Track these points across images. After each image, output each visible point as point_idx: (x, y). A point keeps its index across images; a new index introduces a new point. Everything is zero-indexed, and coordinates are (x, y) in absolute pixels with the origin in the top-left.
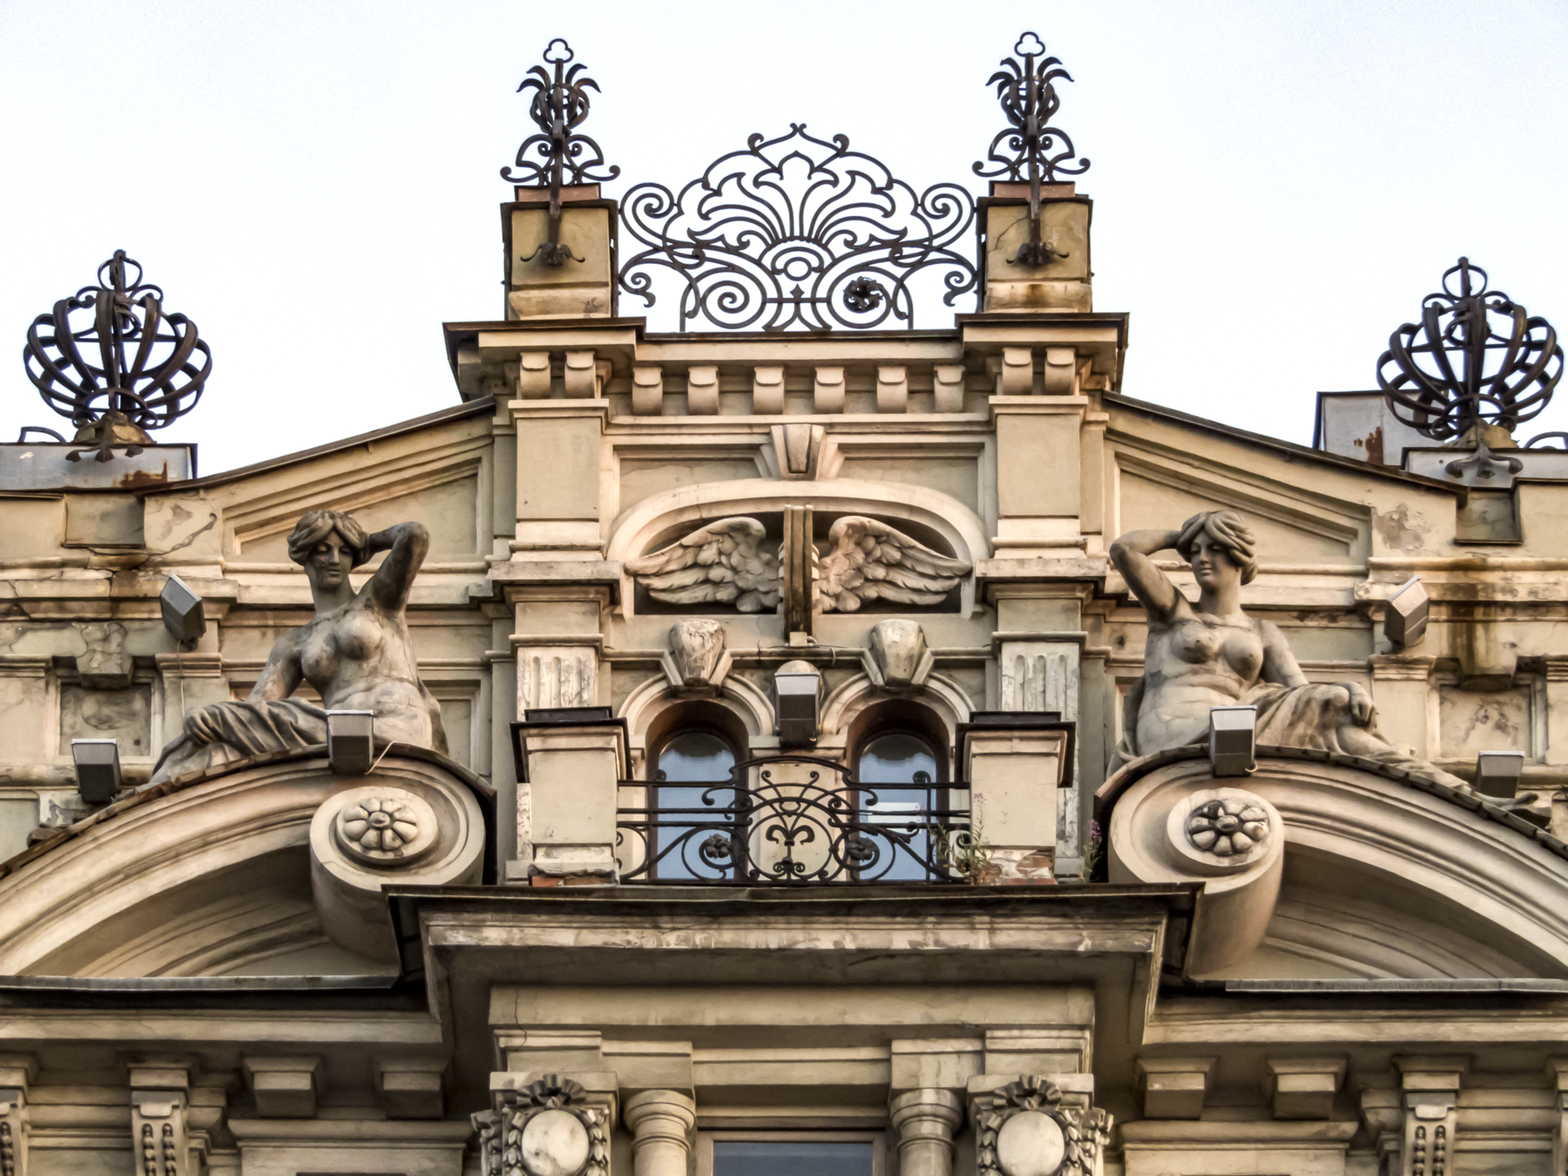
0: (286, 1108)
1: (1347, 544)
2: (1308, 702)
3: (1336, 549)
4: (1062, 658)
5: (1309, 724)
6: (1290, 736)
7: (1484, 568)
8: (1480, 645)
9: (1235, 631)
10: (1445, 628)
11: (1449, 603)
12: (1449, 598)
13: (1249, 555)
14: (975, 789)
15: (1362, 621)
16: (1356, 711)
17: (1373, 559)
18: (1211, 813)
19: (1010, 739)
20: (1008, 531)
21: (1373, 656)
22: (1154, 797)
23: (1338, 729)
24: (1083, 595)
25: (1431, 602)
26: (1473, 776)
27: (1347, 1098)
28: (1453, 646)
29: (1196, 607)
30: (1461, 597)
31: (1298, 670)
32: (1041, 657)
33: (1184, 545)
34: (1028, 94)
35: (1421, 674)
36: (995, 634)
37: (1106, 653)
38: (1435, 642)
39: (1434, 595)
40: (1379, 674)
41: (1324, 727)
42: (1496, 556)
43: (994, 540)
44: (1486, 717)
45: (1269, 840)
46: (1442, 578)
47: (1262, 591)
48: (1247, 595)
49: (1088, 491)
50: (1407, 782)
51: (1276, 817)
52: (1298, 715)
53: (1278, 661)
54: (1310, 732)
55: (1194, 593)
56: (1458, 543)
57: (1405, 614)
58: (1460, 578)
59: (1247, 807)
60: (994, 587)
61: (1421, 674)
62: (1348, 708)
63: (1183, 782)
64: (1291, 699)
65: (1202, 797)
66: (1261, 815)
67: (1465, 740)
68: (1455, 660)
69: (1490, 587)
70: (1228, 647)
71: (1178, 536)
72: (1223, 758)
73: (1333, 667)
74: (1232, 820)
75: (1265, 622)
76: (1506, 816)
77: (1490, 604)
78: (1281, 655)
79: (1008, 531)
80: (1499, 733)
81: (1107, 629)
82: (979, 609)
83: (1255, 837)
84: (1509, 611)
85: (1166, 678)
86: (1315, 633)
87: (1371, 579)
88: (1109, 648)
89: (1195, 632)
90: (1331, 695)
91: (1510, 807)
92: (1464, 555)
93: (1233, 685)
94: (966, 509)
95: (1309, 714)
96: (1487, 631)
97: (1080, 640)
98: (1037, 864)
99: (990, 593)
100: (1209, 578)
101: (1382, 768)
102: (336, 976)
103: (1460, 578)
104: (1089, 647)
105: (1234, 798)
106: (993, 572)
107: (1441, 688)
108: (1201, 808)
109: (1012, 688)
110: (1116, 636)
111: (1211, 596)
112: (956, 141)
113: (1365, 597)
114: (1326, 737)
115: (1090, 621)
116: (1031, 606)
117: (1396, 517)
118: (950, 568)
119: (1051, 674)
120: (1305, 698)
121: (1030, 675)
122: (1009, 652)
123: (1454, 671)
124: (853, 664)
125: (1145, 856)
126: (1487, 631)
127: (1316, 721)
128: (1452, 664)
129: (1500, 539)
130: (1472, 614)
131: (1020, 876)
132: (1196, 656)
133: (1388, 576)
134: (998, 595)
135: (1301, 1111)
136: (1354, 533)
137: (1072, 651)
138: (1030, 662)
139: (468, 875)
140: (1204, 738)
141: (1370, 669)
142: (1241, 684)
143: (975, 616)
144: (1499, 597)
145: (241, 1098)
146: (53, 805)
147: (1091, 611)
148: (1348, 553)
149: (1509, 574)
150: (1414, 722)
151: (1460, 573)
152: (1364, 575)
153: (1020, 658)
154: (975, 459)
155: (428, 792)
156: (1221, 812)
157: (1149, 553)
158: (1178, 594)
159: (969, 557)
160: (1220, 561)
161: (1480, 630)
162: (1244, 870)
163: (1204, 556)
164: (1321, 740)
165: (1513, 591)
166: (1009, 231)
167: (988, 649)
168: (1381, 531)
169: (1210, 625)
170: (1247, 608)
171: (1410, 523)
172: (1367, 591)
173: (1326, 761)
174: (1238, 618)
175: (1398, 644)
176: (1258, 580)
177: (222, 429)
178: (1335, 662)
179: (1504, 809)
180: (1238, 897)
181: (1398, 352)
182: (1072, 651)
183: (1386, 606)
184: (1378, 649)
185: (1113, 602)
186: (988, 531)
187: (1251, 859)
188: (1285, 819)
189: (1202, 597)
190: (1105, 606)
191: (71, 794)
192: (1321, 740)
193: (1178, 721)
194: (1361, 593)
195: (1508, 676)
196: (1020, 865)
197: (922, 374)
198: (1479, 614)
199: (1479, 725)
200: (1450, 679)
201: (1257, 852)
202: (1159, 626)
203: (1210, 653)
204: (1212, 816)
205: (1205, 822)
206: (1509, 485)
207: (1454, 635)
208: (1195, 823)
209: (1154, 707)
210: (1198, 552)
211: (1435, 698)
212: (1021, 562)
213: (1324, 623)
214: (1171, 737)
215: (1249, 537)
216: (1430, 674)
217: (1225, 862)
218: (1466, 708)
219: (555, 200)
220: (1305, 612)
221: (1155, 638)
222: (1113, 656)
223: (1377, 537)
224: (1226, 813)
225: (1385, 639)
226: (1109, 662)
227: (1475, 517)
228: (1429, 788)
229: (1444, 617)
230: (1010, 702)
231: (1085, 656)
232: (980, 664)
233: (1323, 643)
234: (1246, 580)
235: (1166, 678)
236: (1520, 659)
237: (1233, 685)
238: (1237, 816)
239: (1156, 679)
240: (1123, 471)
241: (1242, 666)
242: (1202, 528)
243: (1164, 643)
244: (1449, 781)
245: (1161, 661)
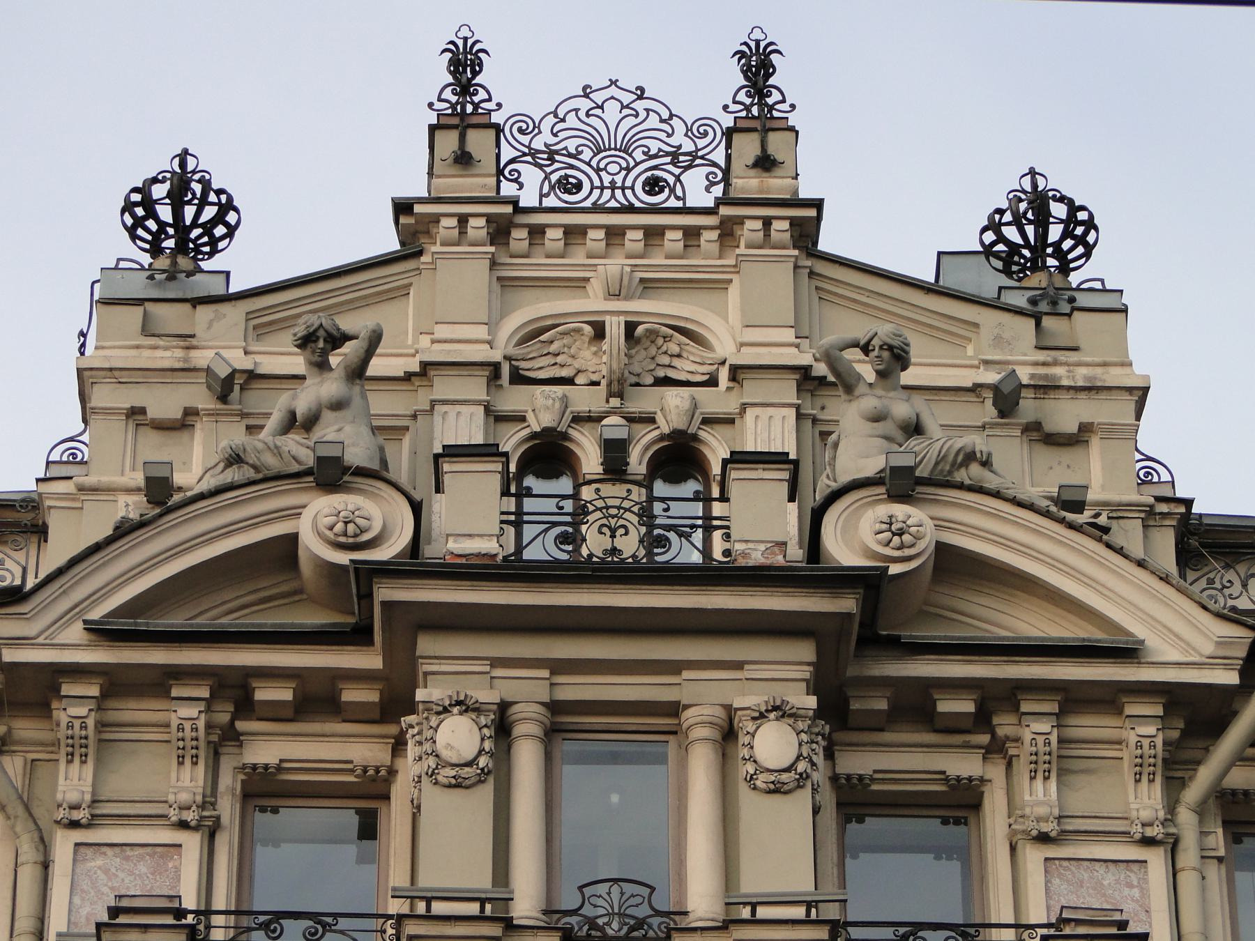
0: (274, 713)
34: (758, 66)
103: (1042, 371)
112: (714, 92)
122: (750, 413)
135: (953, 727)
145: (246, 706)
166: (747, 147)
177: (245, 262)
181: (993, 225)
197: (691, 234)
205: (884, 527)
219: (463, 118)
231: (800, 416)
244: (1044, 503)
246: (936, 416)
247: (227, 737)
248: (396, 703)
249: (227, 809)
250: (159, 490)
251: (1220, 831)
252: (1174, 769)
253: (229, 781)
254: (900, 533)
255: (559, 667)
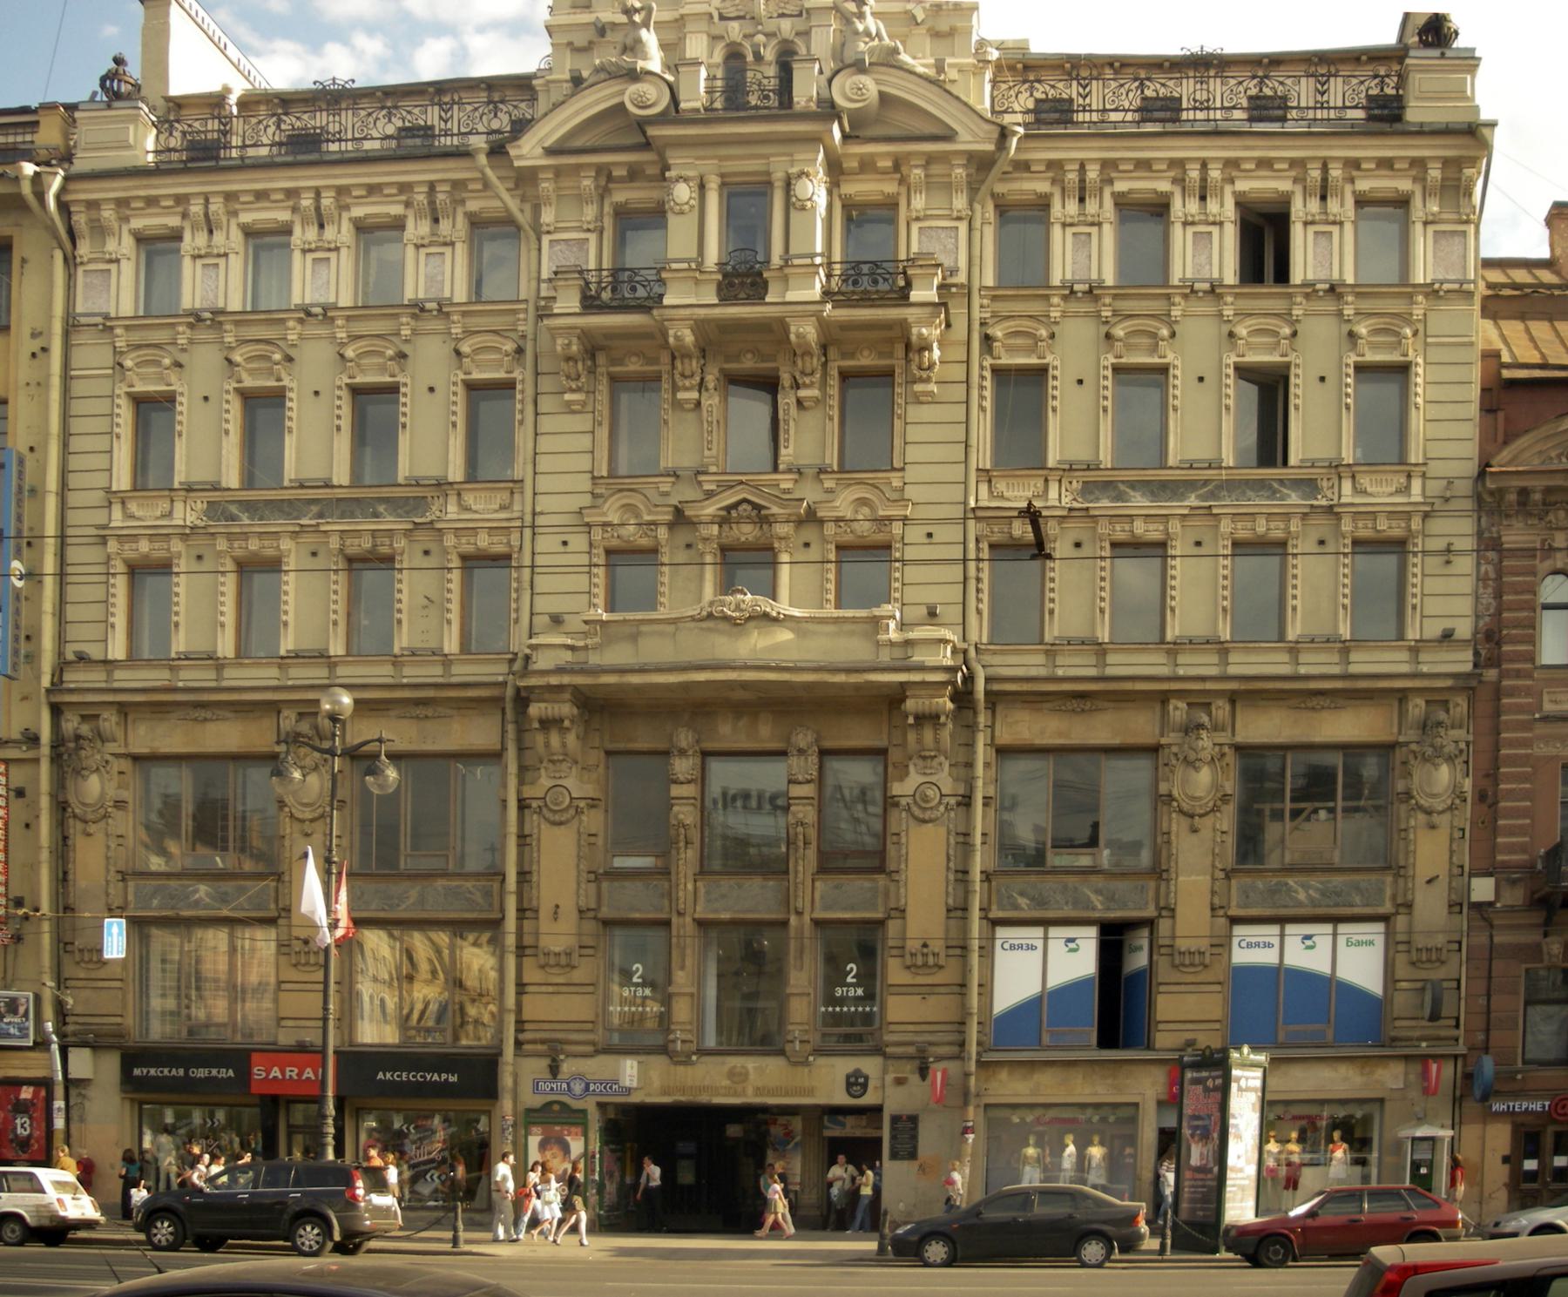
0: (621, 180)
27: (897, 167)
102: (372, 280)
124: (774, 35)
139: (667, 108)
146: (567, 87)
155: (655, 84)
191: (570, 85)
247: (604, 192)
248: (661, 176)
249: (608, 222)
250: (577, 81)
252: (973, 190)
253: (607, 209)
255: (721, 158)
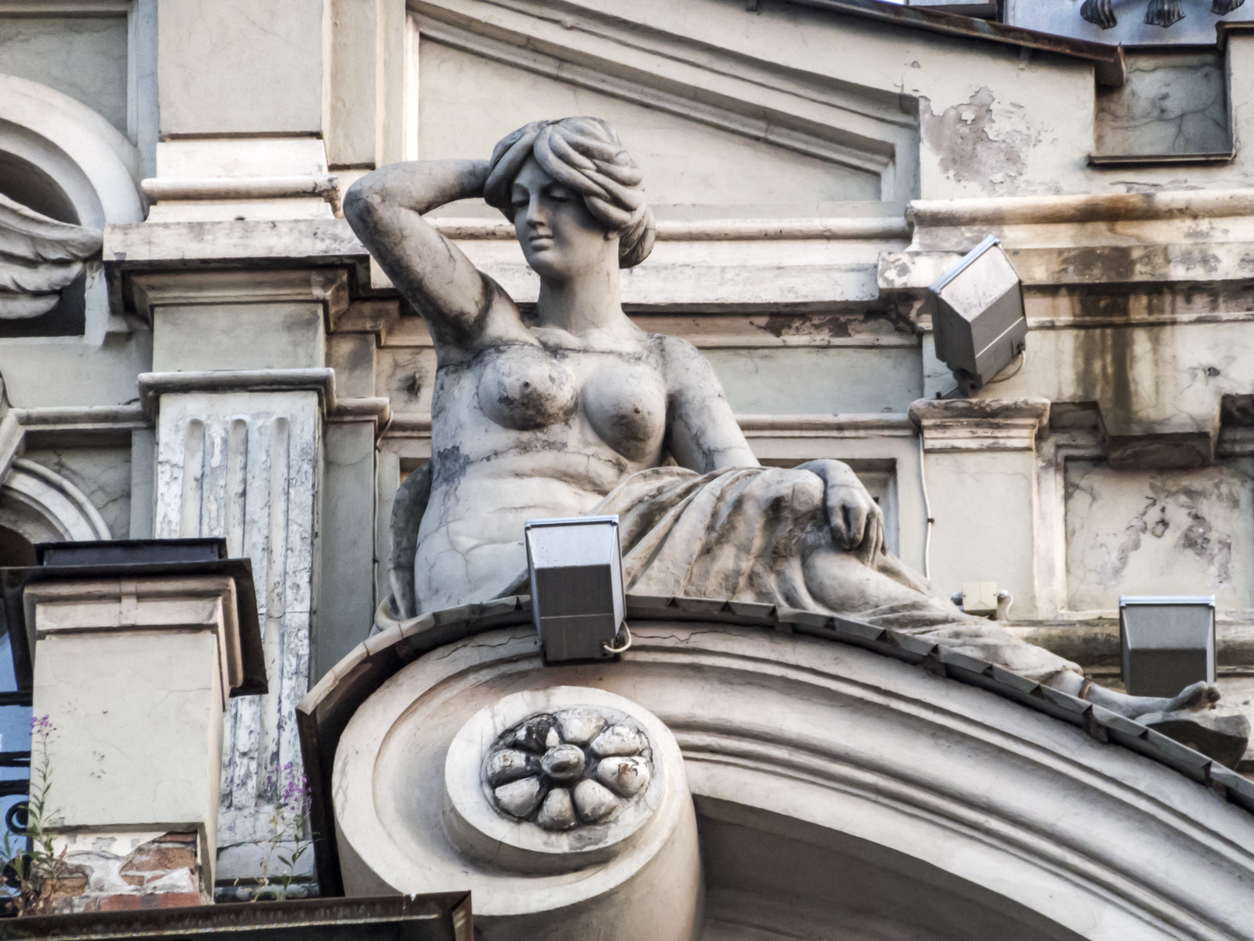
1: (877, 175)
2: (738, 504)
3: (855, 185)
4: (282, 423)
5: (744, 549)
6: (706, 574)
7: (1150, 213)
8: (1143, 373)
9: (607, 361)
10: (1068, 341)
11: (1072, 289)
12: (1072, 278)
13: (629, 208)
14: (37, 710)
15: (899, 331)
16: (838, 521)
17: (919, 205)
18: (531, 739)
19: (117, 598)
20: (176, 166)
21: (919, 404)
22: (424, 710)
23: (805, 557)
24: (328, 294)
25: (1023, 289)
26: (1099, 653)
28: (1085, 378)
29: (529, 313)
30: (1096, 275)
31: (739, 436)
32: (240, 423)
33: (496, 187)
35: (1022, 436)
36: (145, 377)
37: (377, 410)
38: (1049, 368)
39: (1040, 274)
40: (933, 439)
41: (774, 555)
42: (1172, 189)
43: (147, 184)
44: (1164, 523)
45: (651, 795)
46: (1065, 237)
47: (668, 277)
48: (646, 285)
49: (348, 78)
50: (936, 665)
51: (666, 743)
52: (719, 533)
53: (695, 421)
54: (746, 565)
55: (525, 286)
56: (1096, 165)
57: (969, 317)
58: (1100, 237)
59: (606, 726)
60: (142, 281)
61: (1022, 436)
62: (821, 514)
63: (485, 675)
64: (704, 498)
65: (516, 707)
66: (633, 742)
67: (1117, 572)
68: (1088, 405)
69: (1154, 252)
70: (591, 396)
71: (487, 172)
72: (560, 626)
73: (840, 427)
74: (574, 755)
75: (672, 341)
76: (1145, 735)
77: (1158, 289)
78: (704, 407)
79: (176, 166)
80: (1190, 553)
81: (382, 363)
82: (119, 326)
83: (620, 789)
84: (1200, 301)
85: (468, 462)
86: (804, 358)
87: (915, 245)
88: (384, 400)
89: (521, 364)
90: (784, 490)
91: (1157, 717)
92: (1108, 188)
93: (607, 473)
94: (98, 122)
95: (741, 526)
96: (1156, 342)
97: (320, 386)
98: (165, 861)
99: (139, 293)
100: (549, 256)
101: (883, 636)
103: (1100, 237)
104: (342, 399)
105: (579, 707)
106: (140, 253)
107: (1065, 465)
108: (512, 730)
109: (176, 488)
110: (402, 374)
111: (558, 294)
113: (899, 282)
114: (779, 574)
115: (345, 347)
116: (221, 317)
117: (968, 115)
118: (63, 244)
119: (258, 456)
120: (731, 497)
121: (216, 460)
122: (173, 411)
123: (1094, 429)
125: (402, 834)
126: (1156, 342)
127: (758, 543)
128: (1086, 416)
129: (1194, 152)
130: (1125, 311)
131: (127, 889)
132: (525, 414)
133: (950, 237)
134: (153, 296)
136: (889, 152)
137: (305, 408)
138: (216, 433)
140: (521, 588)
141: (915, 429)
142: (621, 469)
143: (112, 340)
144: (1178, 273)
147: (348, 326)
148: (878, 193)
149: (1204, 224)
150: (997, 542)
151: (1102, 226)
152: (904, 237)
153: (196, 424)
154: (124, 16)
156: (552, 737)
157: (423, 210)
158: (489, 288)
159: (101, 220)
160: (568, 221)
161: (1141, 342)
162: (602, 858)
163: (533, 212)
164: (771, 582)
165: (1206, 260)
167: (136, 407)
168: (937, 146)
169: (555, 351)
170: (635, 311)
171: (997, 128)
172: (904, 270)
173: (766, 624)
174: (621, 334)
175: (968, 379)
176: (658, 253)
178: (844, 418)
179: (1142, 722)
180: (595, 918)
182: (305, 408)
183: (932, 301)
184: (931, 388)
185: (393, 307)
186: (139, 167)
187: (613, 835)
188: (684, 747)
189: (542, 296)
190: (375, 317)
192: (771, 582)
193: (488, 548)
194: (892, 274)
195: (1203, 436)
196: (129, 865)
198: (1138, 309)
199: (1147, 539)
200: (1085, 445)
201: (628, 819)
202: (455, 354)
203: (552, 408)
204: (534, 745)
205: (518, 759)
206: (1210, 38)
207: (1087, 353)
208: (498, 763)
209: (443, 522)
210: (525, 204)
211: (1054, 484)
212: (197, 229)
213: (823, 337)
214: (474, 583)
215: (624, 172)
216: (1040, 438)
217: (562, 844)
218: (1119, 504)
220: (781, 317)
221: (448, 381)
222: (392, 416)
223: (929, 158)
224: (563, 740)
225: (942, 367)
226: (385, 430)
227: (1141, 106)
228: (986, 679)
229: (1066, 318)
230: (174, 516)
231: (334, 418)
232: (117, 439)
233: (817, 380)
234: (630, 259)
235: (468, 462)
236: (1228, 402)
237: (607, 473)
238: (584, 745)
239: (451, 464)
240: (423, 37)
241: (621, 432)
242: (529, 153)
243: (465, 388)
244: (1033, 662)
245: (460, 426)
246: (725, 399)
251: (1104, 280)
254: (566, 778)
